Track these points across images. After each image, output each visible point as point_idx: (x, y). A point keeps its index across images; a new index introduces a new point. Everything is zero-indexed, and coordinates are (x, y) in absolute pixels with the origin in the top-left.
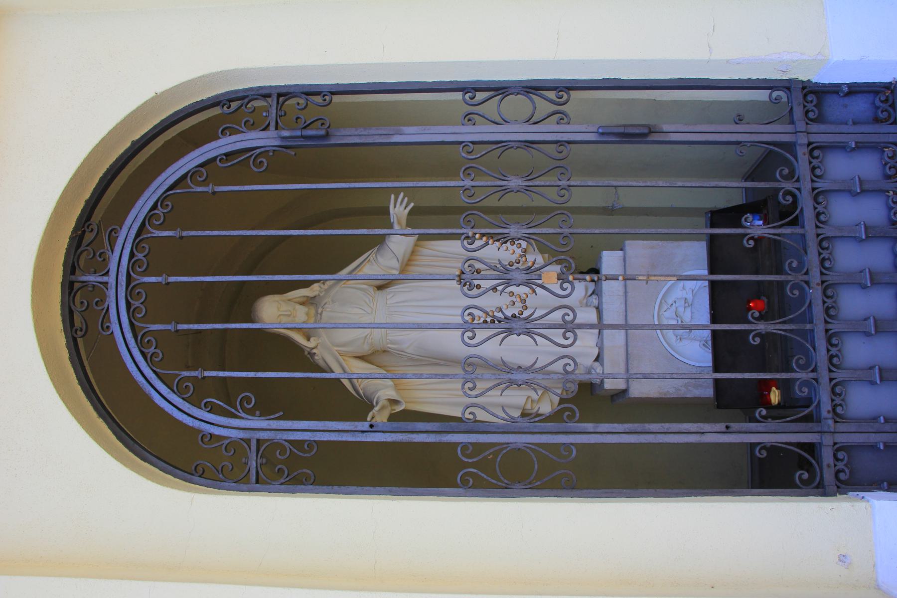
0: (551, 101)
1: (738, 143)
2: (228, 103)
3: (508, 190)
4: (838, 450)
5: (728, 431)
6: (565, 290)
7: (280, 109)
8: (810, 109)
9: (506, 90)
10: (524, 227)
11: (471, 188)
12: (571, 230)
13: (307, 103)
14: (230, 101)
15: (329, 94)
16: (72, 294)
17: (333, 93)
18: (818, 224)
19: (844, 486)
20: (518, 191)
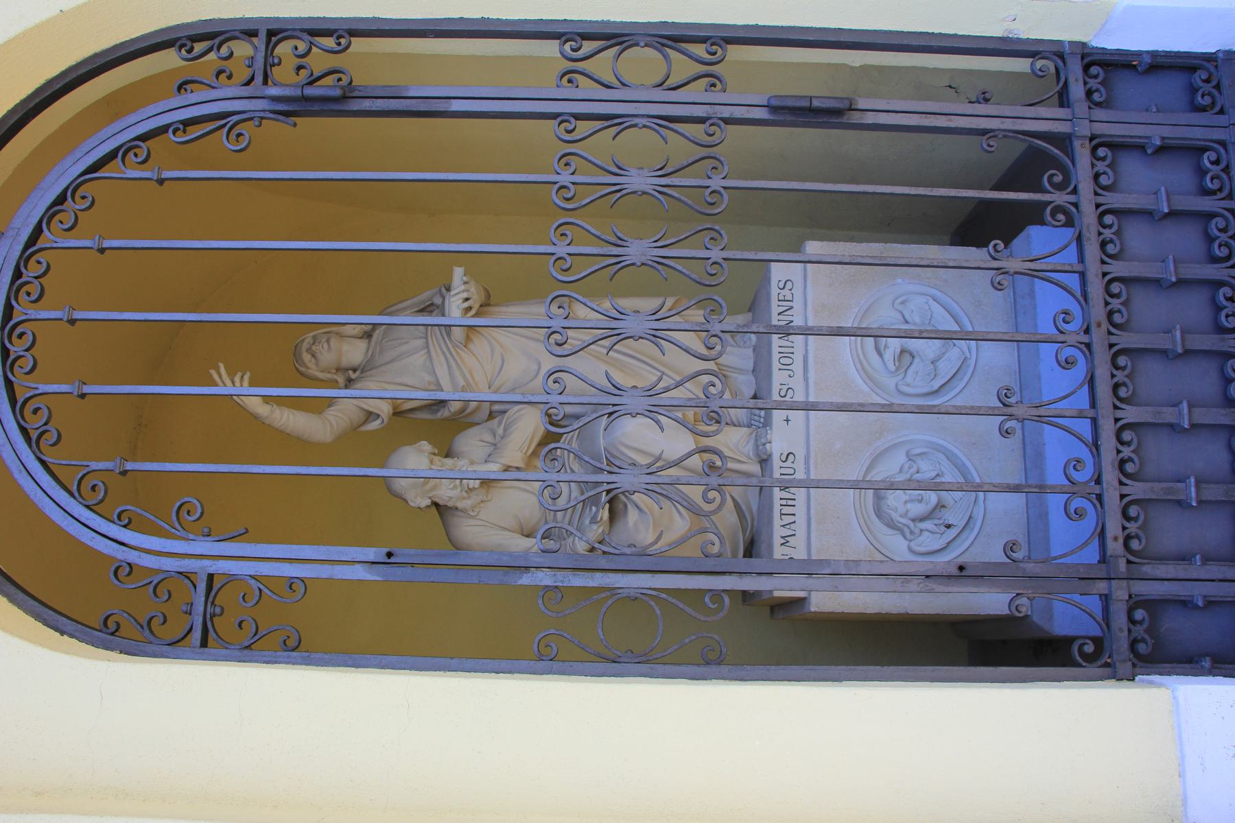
1: (984, 132)
2: (189, 44)
3: (623, 264)
5: (963, 574)
9: (626, 39)
12: (726, 254)
17: (353, 33)
18: (1118, 404)
20: (643, 264)
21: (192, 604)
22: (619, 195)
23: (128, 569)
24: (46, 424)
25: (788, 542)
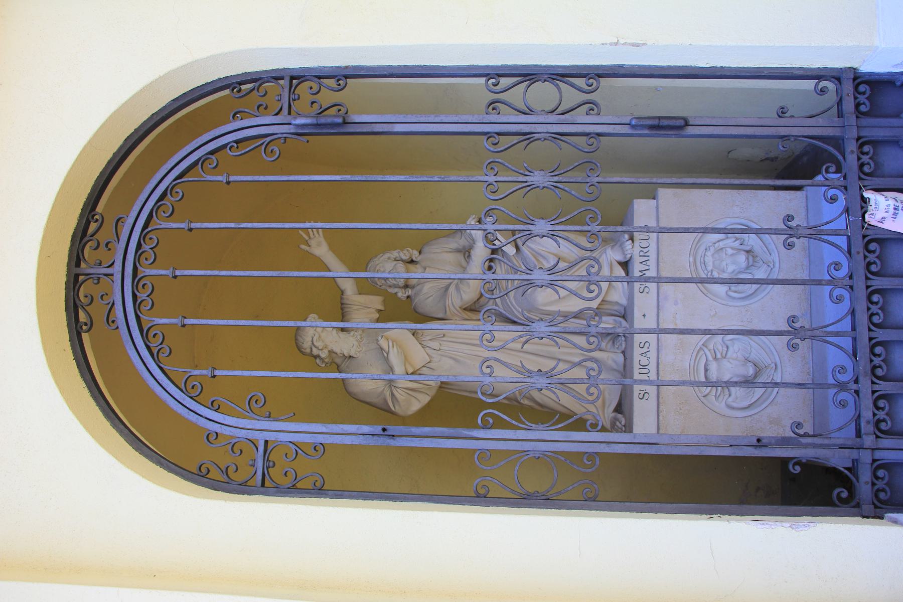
0: (580, 90)
3: (531, 140)
4: (879, 467)
6: (592, 292)
7: (294, 92)
8: (866, 162)
9: (534, 77)
10: (548, 174)
11: (494, 183)
13: (320, 87)
14: (241, 83)
15: (344, 79)
16: (77, 288)
19: (862, 116)
21: (255, 460)
22: (529, 188)
23: (215, 435)
24: (161, 344)
25: (645, 274)
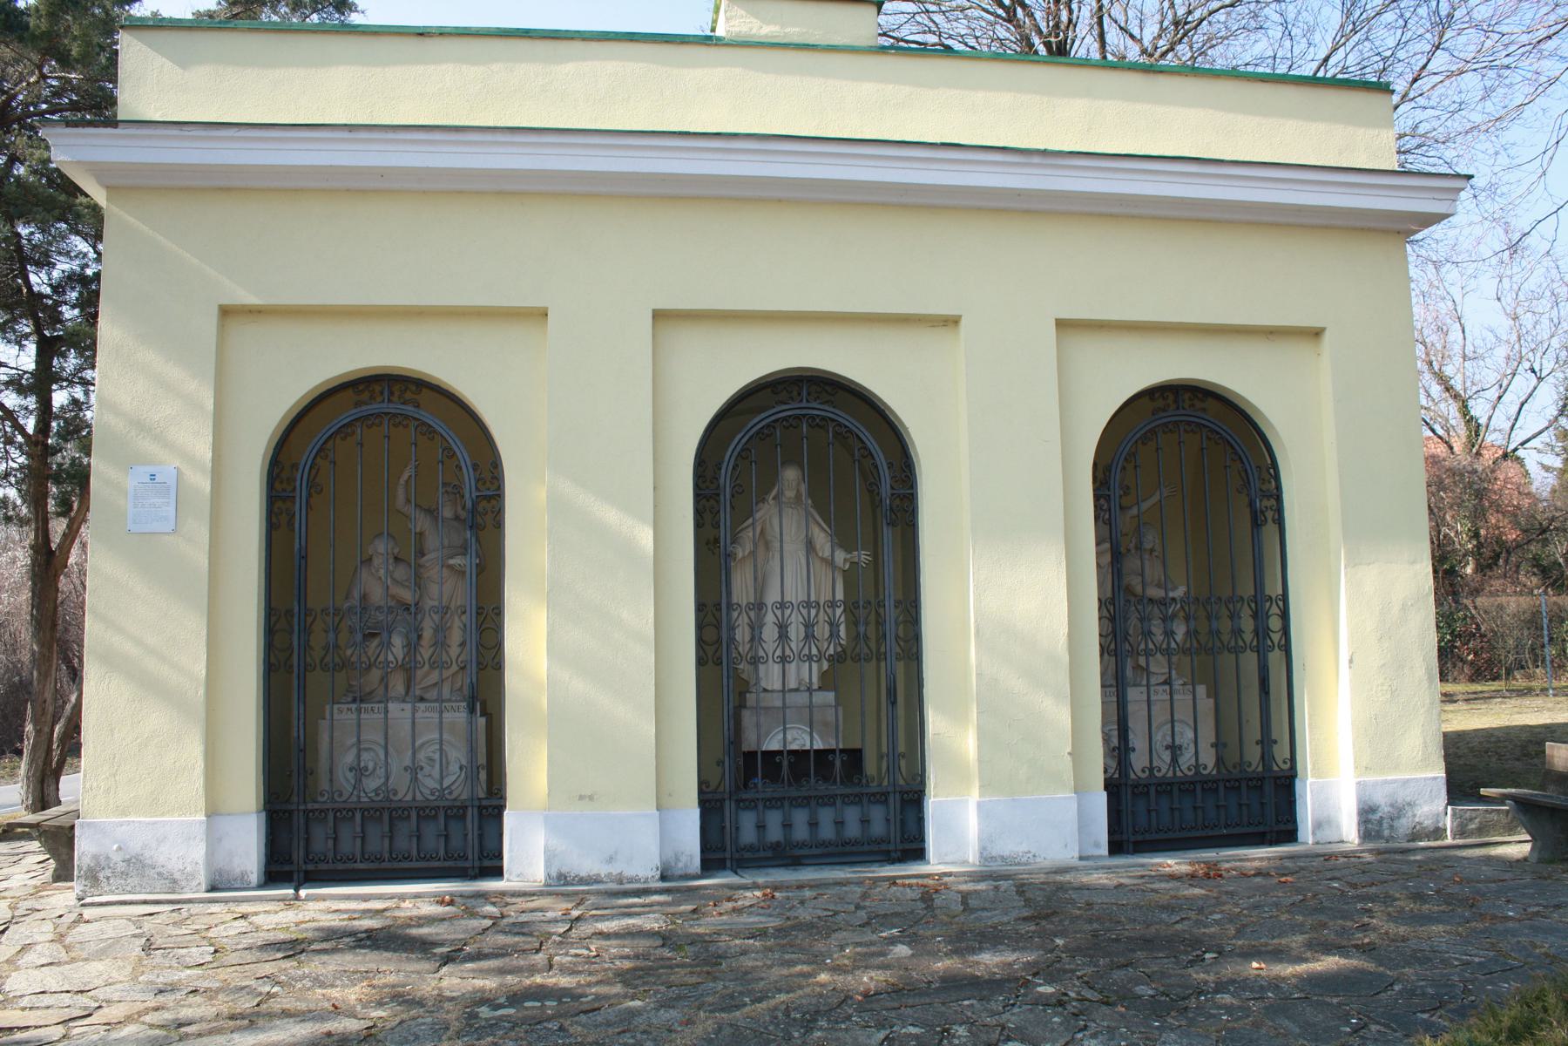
0: (1251, 643)
